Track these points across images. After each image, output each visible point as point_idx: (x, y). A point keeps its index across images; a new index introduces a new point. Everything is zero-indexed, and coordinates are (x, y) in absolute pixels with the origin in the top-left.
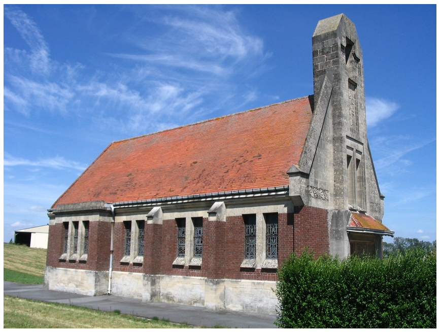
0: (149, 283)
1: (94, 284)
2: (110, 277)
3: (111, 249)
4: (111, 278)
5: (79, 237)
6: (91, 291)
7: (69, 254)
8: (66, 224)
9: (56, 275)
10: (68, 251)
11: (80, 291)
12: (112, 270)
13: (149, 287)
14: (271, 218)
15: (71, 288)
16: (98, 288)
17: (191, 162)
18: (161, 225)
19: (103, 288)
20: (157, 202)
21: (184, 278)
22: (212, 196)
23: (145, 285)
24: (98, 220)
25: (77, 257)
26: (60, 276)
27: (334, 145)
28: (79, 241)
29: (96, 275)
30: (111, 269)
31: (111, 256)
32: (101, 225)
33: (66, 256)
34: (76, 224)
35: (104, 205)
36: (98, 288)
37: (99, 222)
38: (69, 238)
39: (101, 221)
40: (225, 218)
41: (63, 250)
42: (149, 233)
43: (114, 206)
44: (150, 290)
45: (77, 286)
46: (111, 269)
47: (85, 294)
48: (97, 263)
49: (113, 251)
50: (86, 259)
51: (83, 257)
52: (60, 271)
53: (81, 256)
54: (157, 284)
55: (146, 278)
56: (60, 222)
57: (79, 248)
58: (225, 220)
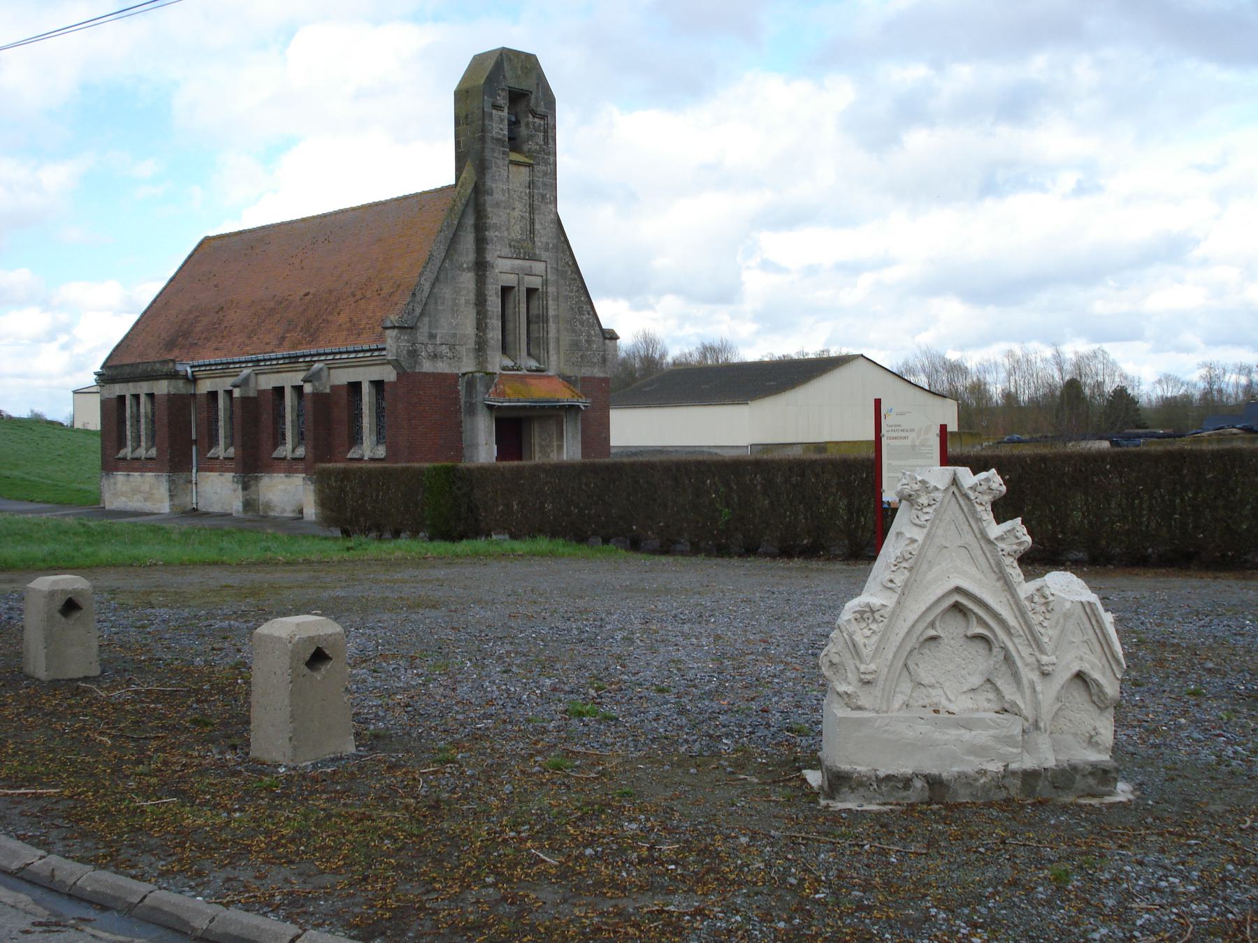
0: (240, 486)
1: (168, 494)
2: (194, 482)
3: (194, 437)
4: (196, 484)
5: (143, 420)
6: (165, 507)
7: (130, 449)
8: (122, 399)
9: (115, 484)
10: (129, 443)
11: (148, 506)
12: (197, 471)
13: (240, 492)
14: (378, 385)
15: (135, 504)
16: (176, 502)
17: (302, 293)
18: (254, 398)
19: (191, 500)
20: (246, 362)
21: (286, 476)
22: (312, 355)
23: (235, 490)
24: (165, 392)
25: (142, 452)
26: (119, 485)
27: (477, 274)
28: (143, 427)
29: (171, 482)
30: (194, 471)
31: (194, 448)
32: (172, 399)
33: (127, 452)
34: (136, 397)
35: (174, 366)
36: (176, 502)
37: (169, 395)
38: (128, 423)
39: (172, 393)
40: (328, 387)
41: (121, 443)
42: (308, 404)
43: (192, 367)
44: (241, 497)
45: (146, 500)
46: (194, 471)
47: (156, 511)
48: (170, 460)
49: (196, 441)
50: (154, 456)
51: (149, 453)
52: (120, 477)
53: (147, 452)
54: (253, 488)
55: (235, 480)
56: (112, 396)
57: (143, 439)
58: (328, 391)
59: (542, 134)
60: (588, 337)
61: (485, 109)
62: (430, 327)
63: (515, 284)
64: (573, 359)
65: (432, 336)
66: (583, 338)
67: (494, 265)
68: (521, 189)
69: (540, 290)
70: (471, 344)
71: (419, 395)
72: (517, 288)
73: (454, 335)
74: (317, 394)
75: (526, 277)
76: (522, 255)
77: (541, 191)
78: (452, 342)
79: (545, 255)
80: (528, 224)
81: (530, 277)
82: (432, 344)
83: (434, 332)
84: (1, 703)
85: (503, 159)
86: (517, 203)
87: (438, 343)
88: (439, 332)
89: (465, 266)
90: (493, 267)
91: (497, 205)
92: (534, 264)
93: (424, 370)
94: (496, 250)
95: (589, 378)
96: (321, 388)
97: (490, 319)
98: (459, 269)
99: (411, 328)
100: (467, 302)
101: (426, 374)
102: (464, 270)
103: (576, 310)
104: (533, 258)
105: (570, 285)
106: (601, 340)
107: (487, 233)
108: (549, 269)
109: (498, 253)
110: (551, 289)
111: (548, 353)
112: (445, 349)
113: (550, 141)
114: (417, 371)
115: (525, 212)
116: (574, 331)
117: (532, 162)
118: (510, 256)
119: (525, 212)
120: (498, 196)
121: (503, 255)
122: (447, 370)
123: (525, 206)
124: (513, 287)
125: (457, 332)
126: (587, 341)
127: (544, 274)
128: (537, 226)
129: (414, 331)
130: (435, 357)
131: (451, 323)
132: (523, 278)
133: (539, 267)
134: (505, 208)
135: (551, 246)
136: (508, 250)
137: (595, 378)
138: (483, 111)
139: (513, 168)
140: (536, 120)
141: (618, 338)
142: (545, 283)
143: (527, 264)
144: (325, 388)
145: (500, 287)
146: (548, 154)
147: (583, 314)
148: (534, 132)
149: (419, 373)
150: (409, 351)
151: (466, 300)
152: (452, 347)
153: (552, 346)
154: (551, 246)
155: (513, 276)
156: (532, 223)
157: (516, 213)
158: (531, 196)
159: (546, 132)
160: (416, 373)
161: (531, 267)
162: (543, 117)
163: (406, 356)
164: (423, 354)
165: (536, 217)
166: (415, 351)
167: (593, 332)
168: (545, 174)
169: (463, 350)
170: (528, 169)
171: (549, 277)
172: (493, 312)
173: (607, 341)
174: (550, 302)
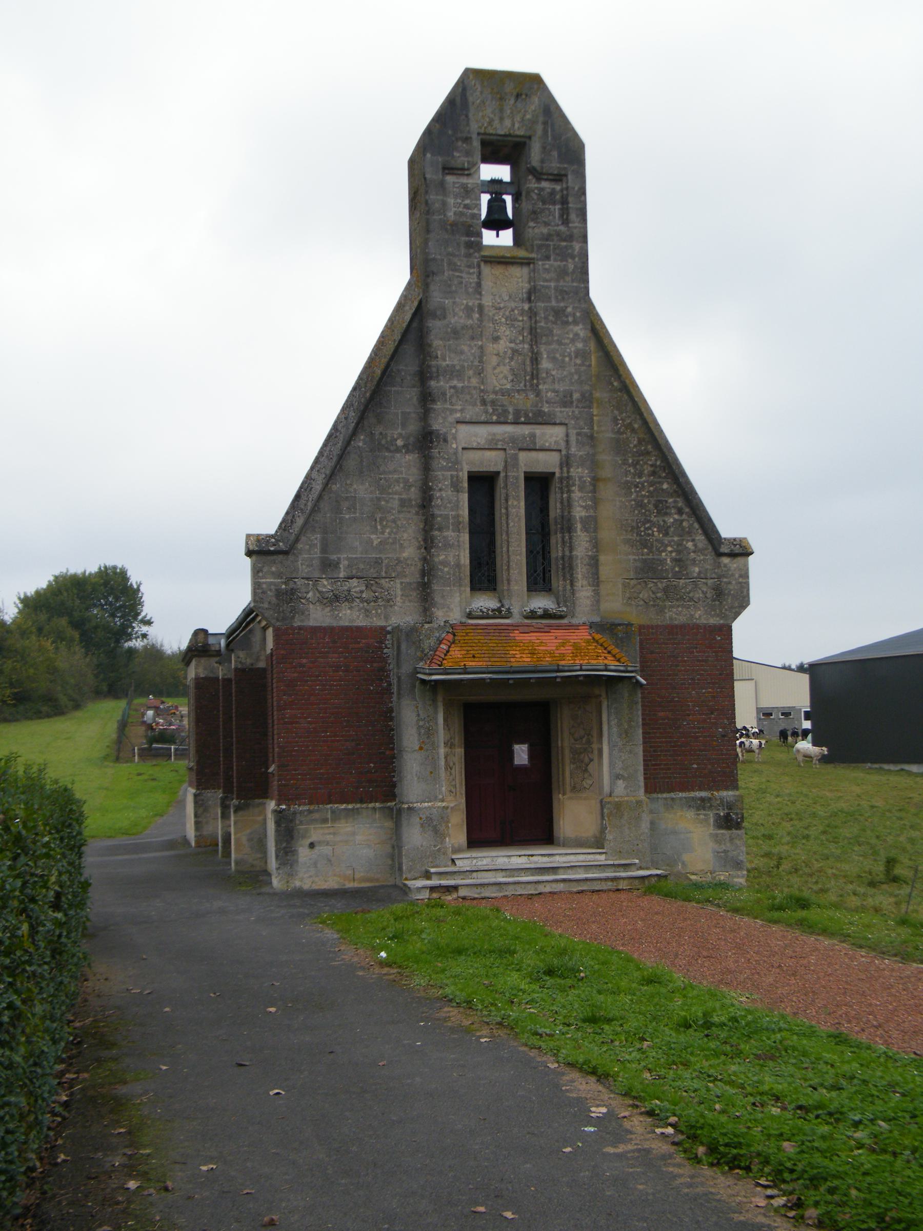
39: (202, 676)
58: (262, 665)
59: (558, 207)
60: (679, 552)
61: (428, 176)
62: (324, 550)
63: (500, 468)
64: (644, 595)
65: (328, 565)
66: (668, 556)
67: (450, 438)
68: (513, 305)
69: (557, 475)
70: (412, 575)
71: (302, 666)
72: (502, 475)
73: (378, 562)
74: (243, 670)
75: (523, 456)
76: (511, 417)
77: (554, 303)
78: (372, 572)
79: (560, 413)
80: (528, 362)
81: (533, 454)
82: (328, 579)
83: (334, 557)
84: (922, 1069)
85: (468, 256)
86: (503, 328)
87: (342, 575)
88: (344, 558)
89: (400, 443)
90: (445, 440)
91: (456, 333)
92: (538, 430)
93: (312, 623)
94: (452, 411)
95: (682, 627)
96: (249, 661)
97: (440, 529)
98: (388, 450)
99: (285, 553)
100: (403, 503)
101: (315, 630)
102: (398, 450)
103: (651, 506)
104: (540, 419)
105: (634, 465)
106: (710, 557)
107: (433, 383)
108: (573, 438)
109: (458, 415)
110: (579, 472)
111: (572, 585)
112: (355, 586)
113: (573, 216)
114: (297, 624)
115: (523, 342)
116: (644, 544)
117: (533, 255)
118: (483, 418)
119: (523, 342)
120: (458, 319)
121: (468, 417)
122: (361, 622)
123: (521, 332)
124: (498, 473)
125: (383, 556)
126: (677, 561)
127: (562, 445)
128: (545, 364)
129: (291, 557)
130: (334, 600)
131: (370, 541)
132: (515, 458)
133: (552, 435)
134: (472, 338)
135: (576, 396)
136: (479, 408)
137: (697, 626)
138: (425, 179)
139: (486, 270)
140: (544, 184)
141: (752, 553)
142: (566, 462)
143: (526, 430)
144: (258, 659)
145: (522, 476)
146: (570, 238)
147: (666, 514)
148: (540, 204)
149: (300, 628)
150: (279, 593)
151: (401, 500)
152: (370, 582)
153: (581, 571)
154: (576, 396)
155: (493, 453)
156: (535, 359)
157: (503, 345)
158: (532, 314)
159: (564, 202)
160: (293, 628)
161: (533, 436)
162: (558, 178)
163: (274, 600)
164: (310, 595)
165: (543, 348)
166: (293, 591)
167: (690, 545)
168: (562, 273)
169: (397, 587)
170: (525, 270)
171: (573, 450)
172: (446, 517)
173: (726, 560)
174: (577, 494)
